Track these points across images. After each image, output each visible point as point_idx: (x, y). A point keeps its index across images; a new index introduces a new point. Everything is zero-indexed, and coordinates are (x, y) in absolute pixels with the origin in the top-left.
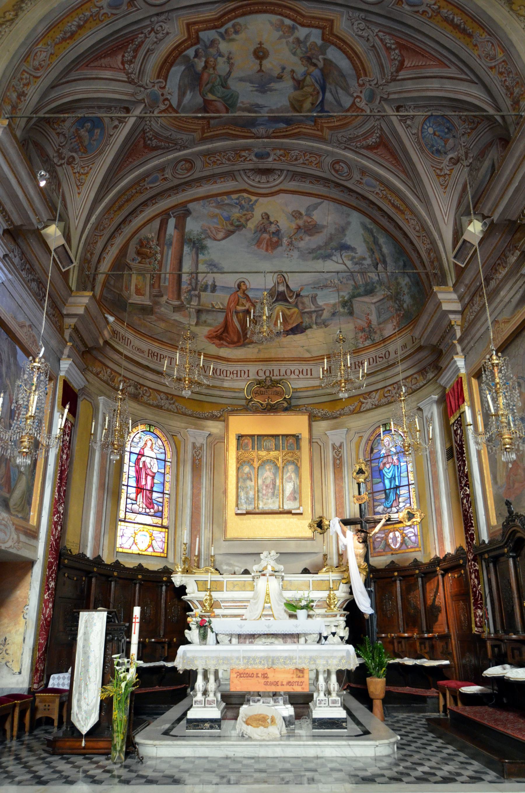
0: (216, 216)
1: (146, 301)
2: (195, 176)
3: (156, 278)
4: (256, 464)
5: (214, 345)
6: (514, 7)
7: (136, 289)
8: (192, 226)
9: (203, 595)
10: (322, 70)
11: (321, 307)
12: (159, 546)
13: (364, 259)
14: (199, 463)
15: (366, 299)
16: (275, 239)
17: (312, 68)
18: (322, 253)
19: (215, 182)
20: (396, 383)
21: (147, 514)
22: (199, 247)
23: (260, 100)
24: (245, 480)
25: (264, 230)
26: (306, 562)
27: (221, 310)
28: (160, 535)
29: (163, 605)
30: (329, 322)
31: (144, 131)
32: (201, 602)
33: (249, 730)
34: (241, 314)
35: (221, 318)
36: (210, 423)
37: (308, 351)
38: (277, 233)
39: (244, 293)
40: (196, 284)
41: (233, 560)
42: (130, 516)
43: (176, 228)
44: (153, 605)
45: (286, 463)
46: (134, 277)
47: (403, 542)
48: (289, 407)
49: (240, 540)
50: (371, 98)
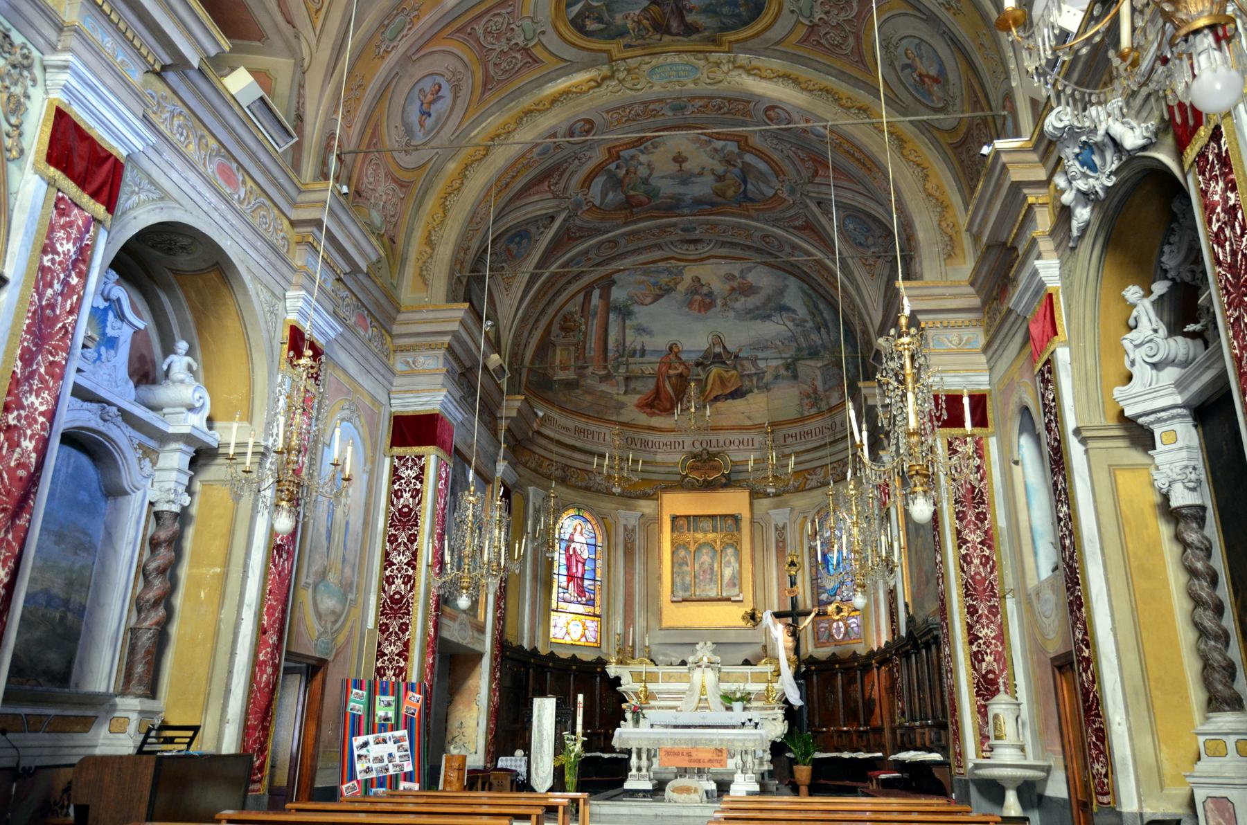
0: (643, 282)
1: (571, 375)
2: (620, 251)
3: (581, 349)
4: (692, 548)
7: (562, 366)
8: (617, 294)
9: (639, 687)
12: (591, 636)
13: (806, 321)
14: (630, 547)
15: (811, 363)
16: (708, 300)
18: (760, 314)
21: (579, 603)
22: (625, 312)
23: (681, 190)
24: (680, 565)
25: (695, 292)
26: (747, 653)
27: (651, 376)
28: (592, 624)
29: (598, 697)
31: (568, 229)
32: (636, 694)
33: (675, 796)
35: (651, 384)
36: (642, 502)
37: (749, 418)
38: (710, 294)
41: (669, 650)
42: (562, 605)
44: (594, 693)
45: (725, 546)
46: (558, 352)
47: (846, 633)
48: (728, 482)
49: (676, 629)
50: (793, 191)
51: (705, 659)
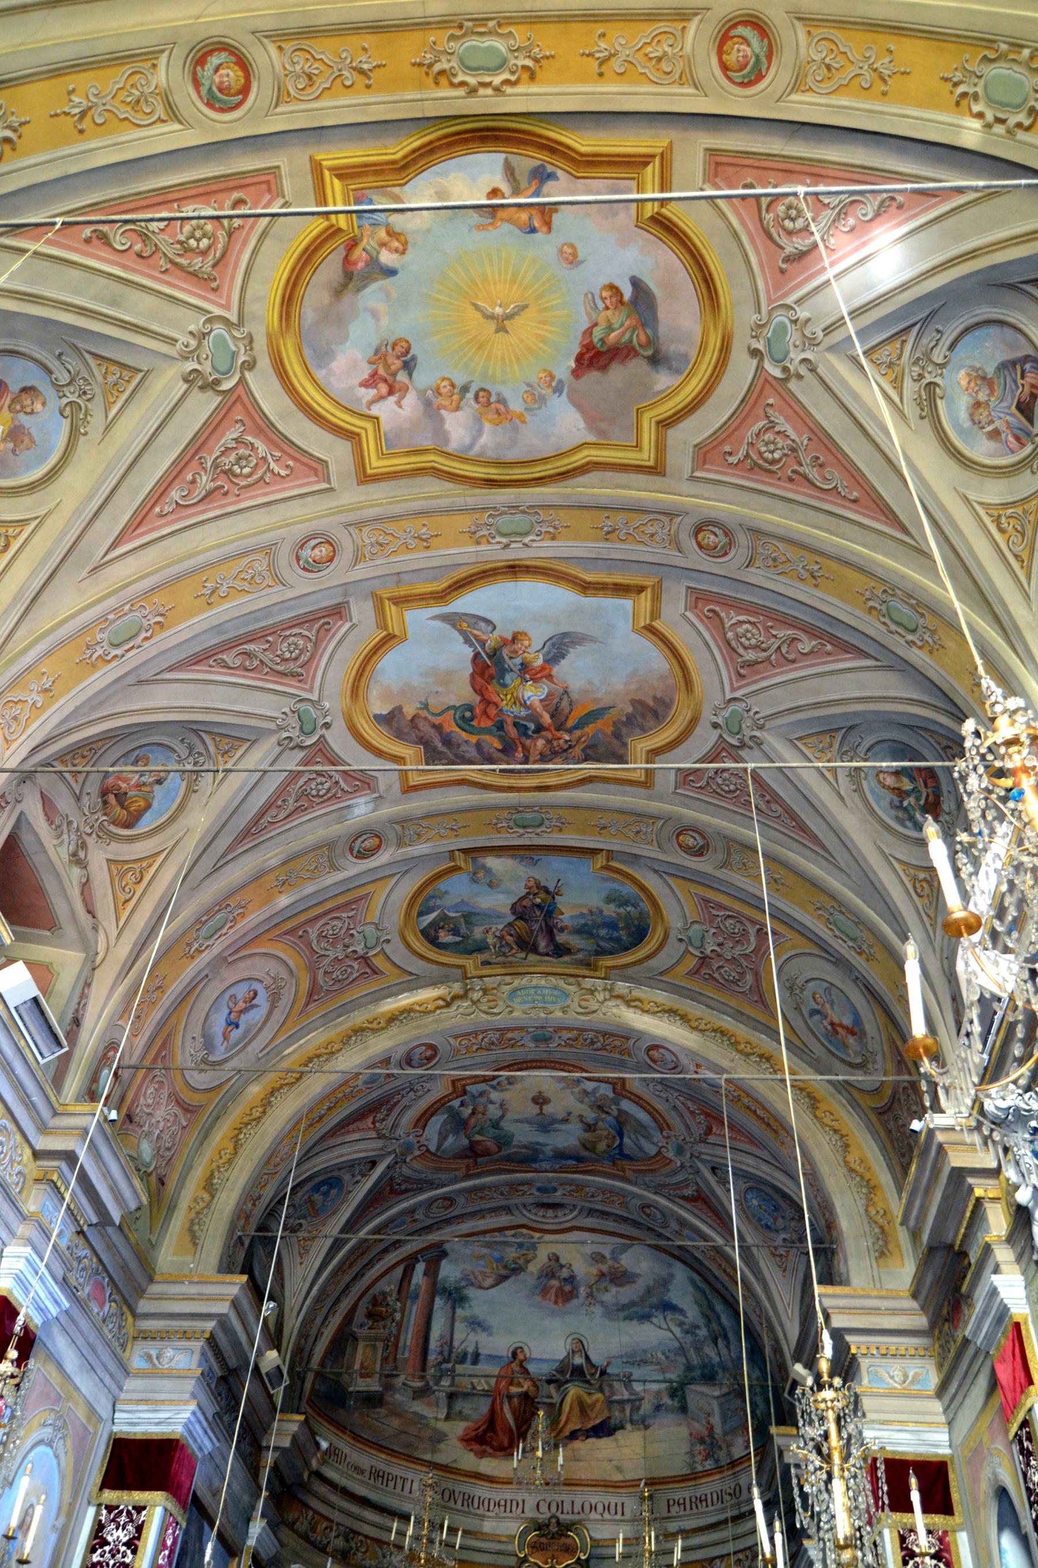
0: (482, 1257)
1: (373, 1385)
2: (455, 1213)
3: (392, 1345)
5: (472, 1454)
6: (818, 1113)
8: (449, 1271)
10: (616, 1118)
11: (637, 1394)
13: (698, 1327)
16: (568, 1288)
17: (604, 1116)
19: (483, 1217)
20: (749, 1548)
22: (456, 1297)
23: (542, 1138)
25: (552, 1275)
27: (485, 1394)
30: (652, 1421)
31: (392, 1179)
34: (515, 1400)
35: (484, 1406)
37: (619, 1469)
38: (571, 1279)
39: (521, 1366)
40: (450, 1352)
43: (425, 1274)
50: (680, 1151)
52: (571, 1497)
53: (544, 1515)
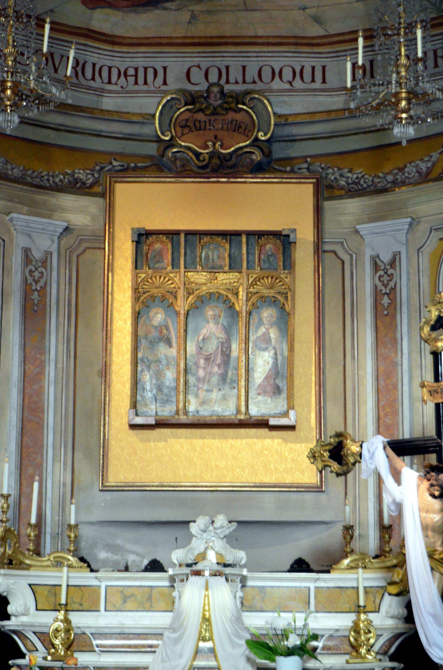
4: (182, 305)
9: (51, 620)
24: (153, 344)
26: (302, 544)
32: (44, 637)
36: (67, 200)
37: (317, 20)
41: (123, 538)
45: (258, 302)
48: (267, 163)
49: (141, 489)
51: (212, 557)
52: (241, 61)
53: (199, 85)
